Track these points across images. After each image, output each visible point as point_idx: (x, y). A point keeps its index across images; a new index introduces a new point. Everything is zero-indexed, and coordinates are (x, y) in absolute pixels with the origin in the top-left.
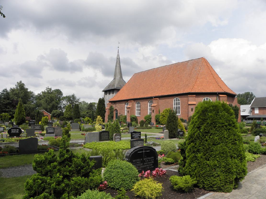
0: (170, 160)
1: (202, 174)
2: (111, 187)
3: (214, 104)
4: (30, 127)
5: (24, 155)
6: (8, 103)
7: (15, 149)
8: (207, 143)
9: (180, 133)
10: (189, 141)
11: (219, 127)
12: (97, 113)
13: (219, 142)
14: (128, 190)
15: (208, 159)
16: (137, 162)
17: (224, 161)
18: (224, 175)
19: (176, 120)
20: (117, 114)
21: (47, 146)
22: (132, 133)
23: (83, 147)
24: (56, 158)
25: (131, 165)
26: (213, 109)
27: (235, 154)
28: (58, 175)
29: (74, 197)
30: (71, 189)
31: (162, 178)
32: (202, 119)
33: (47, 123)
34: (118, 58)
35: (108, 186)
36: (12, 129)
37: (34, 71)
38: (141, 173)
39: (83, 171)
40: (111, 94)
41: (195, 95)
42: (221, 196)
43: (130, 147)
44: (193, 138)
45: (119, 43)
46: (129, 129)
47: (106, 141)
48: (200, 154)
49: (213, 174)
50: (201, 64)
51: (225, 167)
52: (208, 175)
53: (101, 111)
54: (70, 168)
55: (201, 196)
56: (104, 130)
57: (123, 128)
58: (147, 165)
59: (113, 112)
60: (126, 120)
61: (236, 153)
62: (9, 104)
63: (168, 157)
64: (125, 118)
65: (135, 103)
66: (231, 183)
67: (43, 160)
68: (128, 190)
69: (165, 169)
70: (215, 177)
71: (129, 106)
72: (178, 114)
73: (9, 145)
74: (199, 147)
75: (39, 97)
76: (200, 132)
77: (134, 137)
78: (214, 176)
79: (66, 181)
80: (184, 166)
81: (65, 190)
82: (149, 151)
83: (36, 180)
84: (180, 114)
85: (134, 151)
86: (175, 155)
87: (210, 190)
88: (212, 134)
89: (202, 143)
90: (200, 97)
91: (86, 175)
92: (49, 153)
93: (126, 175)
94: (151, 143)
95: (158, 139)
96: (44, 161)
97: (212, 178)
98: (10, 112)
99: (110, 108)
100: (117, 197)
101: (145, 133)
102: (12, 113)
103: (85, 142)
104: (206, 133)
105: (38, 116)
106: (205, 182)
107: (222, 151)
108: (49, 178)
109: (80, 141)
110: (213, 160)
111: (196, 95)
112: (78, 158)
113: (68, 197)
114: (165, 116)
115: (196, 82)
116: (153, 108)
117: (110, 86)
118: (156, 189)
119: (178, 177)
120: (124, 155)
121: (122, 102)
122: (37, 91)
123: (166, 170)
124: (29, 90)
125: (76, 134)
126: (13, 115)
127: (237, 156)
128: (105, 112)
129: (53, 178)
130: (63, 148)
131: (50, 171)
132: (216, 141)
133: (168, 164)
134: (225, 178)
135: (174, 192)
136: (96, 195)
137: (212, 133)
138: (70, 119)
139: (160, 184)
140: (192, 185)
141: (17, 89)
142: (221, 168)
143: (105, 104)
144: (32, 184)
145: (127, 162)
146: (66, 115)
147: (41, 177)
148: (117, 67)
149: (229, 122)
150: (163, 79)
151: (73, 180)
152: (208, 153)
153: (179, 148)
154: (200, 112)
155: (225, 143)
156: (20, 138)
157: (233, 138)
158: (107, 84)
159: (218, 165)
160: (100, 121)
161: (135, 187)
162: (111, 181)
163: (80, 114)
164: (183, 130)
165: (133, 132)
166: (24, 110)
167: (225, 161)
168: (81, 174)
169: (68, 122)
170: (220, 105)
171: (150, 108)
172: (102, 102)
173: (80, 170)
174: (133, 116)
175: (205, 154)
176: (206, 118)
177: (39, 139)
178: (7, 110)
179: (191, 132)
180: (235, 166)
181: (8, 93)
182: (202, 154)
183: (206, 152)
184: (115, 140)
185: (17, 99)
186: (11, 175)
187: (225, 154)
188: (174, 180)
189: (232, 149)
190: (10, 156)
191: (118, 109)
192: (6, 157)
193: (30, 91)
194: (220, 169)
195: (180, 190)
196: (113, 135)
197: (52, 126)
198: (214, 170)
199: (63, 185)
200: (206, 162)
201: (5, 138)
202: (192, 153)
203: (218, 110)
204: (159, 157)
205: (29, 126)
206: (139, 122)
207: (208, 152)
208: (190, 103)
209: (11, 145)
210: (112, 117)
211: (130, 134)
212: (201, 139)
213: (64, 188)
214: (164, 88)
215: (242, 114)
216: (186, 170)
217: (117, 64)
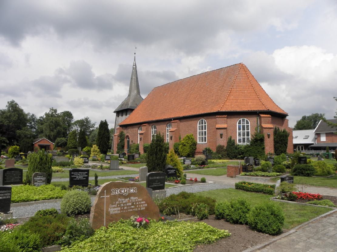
20: (128, 142)
34: (135, 68)
40: (124, 116)
45: (136, 48)
47: (13, 184)
59: (124, 139)
60: (139, 150)
65: (151, 127)
72: (204, 142)
75: (41, 122)
90: (234, 118)
99: (120, 134)
115: (229, 97)
146: (69, 145)
158: (120, 103)
185: (7, 124)
208: (218, 126)
215: (295, 141)
217: (133, 76)
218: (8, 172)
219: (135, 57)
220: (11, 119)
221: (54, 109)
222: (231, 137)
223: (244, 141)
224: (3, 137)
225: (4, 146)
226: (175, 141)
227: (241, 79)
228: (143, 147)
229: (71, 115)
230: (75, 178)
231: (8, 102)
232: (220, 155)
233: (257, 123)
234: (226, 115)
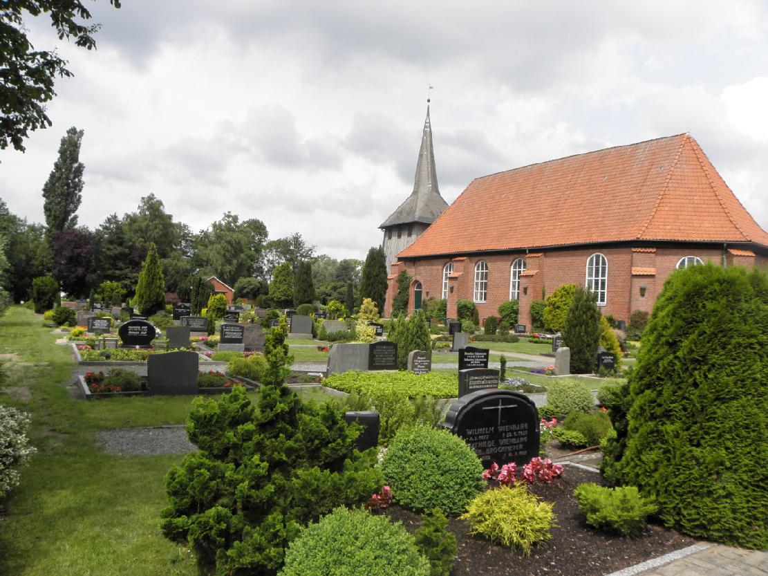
0: (574, 436)
1: (677, 486)
2: (401, 503)
3: (724, 273)
4: (177, 323)
5: (161, 397)
6: (121, 254)
7: (138, 379)
8: (697, 392)
9: (603, 358)
11: (740, 345)
12: (362, 288)
13: (735, 392)
14: (453, 515)
15: (695, 441)
16: (478, 436)
17: (749, 453)
18: (745, 493)
19: (595, 321)
20: (418, 294)
21: (223, 376)
22: (461, 352)
24: (253, 410)
25: (463, 443)
26: (722, 290)
28: (256, 458)
29: (298, 525)
30: (291, 502)
31: (548, 487)
33: (221, 312)
35: (394, 501)
36: (467, 352)
37: (202, 165)
38: (490, 469)
39: (328, 452)
42: (735, 559)
43: (457, 392)
44: (651, 376)
46: (453, 341)
47: (387, 369)
48: (672, 423)
49: (711, 489)
50: (679, 154)
51: (751, 471)
52: (695, 490)
54: (290, 443)
55: (671, 551)
56: (384, 338)
57: (436, 336)
58: (508, 445)
59: (408, 288)
60: (445, 313)
62: (121, 257)
63: (569, 428)
64: (443, 308)
65: (474, 264)
67: (215, 413)
68: (453, 515)
69: (560, 462)
70: (718, 497)
71: (453, 274)
73: (121, 367)
74: (671, 403)
75: (203, 240)
76: (677, 357)
77: (469, 362)
78: (715, 496)
79: (277, 476)
80: (618, 458)
81: (275, 504)
82: (515, 406)
83: (196, 470)
84: (605, 303)
85: (472, 402)
86: (591, 422)
88: (713, 365)
89: (680, 393)
91: (336, 465)
92: (231, 397)
93: (447, 472)
94: (519, 383)
96: (218, 416)
97: (707, 500)
98: (123, 279)
99: (399, 276)
100: (421, 534)
101: (500, 353)
103: (328, 370)
104: (695, 361)
105: (198, 294)
106: (682, 509)
107: (745, 420)
108: (232, 466)
110: (714, 446)
112: (313, 414)
113: (282, 522)
114: (558, 307)
116: (524, 282)
118: (535, 520)
119: (600, 489)
120: (439, 413)
123: (563, 466)
125: (301, 348)
126: (133, 289)
128: (386, 287)
129: (243, 466)
130: (271, 384)
131: (235, 446)
132: (726, 390)
133: (567, 446)
134: (750, 505)
135: (587, 531)
136: (362, 523)
137: (715, 362)
138: (286, 303)
139: (545, 505)
140: (642, 517)
142: (739, 471)
143: (387, 264)
144: (185, 480)
145: (451, 434)
147: (210, 463)
148: (424, 158)
151: (297, 477)
152: (699, 425)
153: (601, 402)
154: (680, 298)
155: (754, 396)
156: (152, 352)
158: (394, 209)
159: (728, 464)
161: (473, 509)
162: (404, 485)
163: (314, 291)
164: (612, 352)
165: (467, 348)
166: (162, 276)
167: (753, 453)
168: (321, 461)
169: (280, 314)
170: (744, 279)
172: (376, 258)
173: (318, 449)
174: (463, 302)
175: (688, 425)
177: (203, 357)
179: (647, 357)
181: (119, 228)
182: (678, 425)
184: (413, 370)
185: (142, 245)
186: (129, 449)
187: (754, 431)
188: (588, 497)
190: (125, 399)
192: (113, 401)
193: (180, 223)
194: (734, 476)
195: (605, 528)
197: (237, 321)
199: (271, 488)
200: (691, 451)
201: (112, 350)
202: (646, 421)
203: (739, 293)
204: (543, 427)
205: (173, 319)
206: (481, 322)
207: (699, 420)
208: (636, 270)
209: (128, 369)
210: (406, 304)
211: (458, 353)
213: (272, 497)
214: (560, 223)
216: (626, 470)
218: (378, 347)
219: (429, 107)
220: (148, 235)
221: (233, 214)
226: (533, 298)
229: (264, 228)
231: (143, 198)
234: (653, 247)
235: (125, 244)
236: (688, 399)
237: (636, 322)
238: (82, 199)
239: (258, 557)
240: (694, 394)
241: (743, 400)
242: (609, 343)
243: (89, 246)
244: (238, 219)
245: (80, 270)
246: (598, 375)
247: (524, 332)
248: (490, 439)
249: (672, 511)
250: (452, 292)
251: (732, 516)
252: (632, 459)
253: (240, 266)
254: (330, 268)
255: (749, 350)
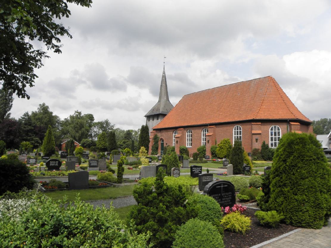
0: (246, 197)
1: (290, 209)
8: (294, 177)
10: (274, 175)
11: (307, 160)
18: (313, 210)
19: (242, 153)
20: (162, 144)
23: (137, 183)
26: (300, 142)
27: (324, 188)
32: (288, 152)
36: (51, 161)
41: (260, 122)
48: (287, 188)
53: (145, 141)
59: (158, 141)
61: (325, 188)
63: (242, 194)
64: (173, 150)
65: (186, 131)
66: (321, 219)
71: (177, 135)
72: (274, 147)
75: (66, 123)
76: (287, 165)
78: (303, 211)
85: (212, 186)
87: (298, 225)
95: (221, 175)
97: (301, 213)
98: (31, 140)
102: (35, 142)
104: (293, 166)
109: (134, 176)
111: (261, 122)
114: (222, 148)
117: (154, 111)
121: (169, 130)
122: (63, 115)
124: (53, 115)
127: (327, 191)
128: (149, 142)
134: (314, 214)
141: (40, 113)
142: (310, 202)
146: (98, 146)
148: (163, 87)
149: (318, 155)
150: (220, 102)
152: (296, 188)
154: (286, 145)
157: (322, 172)
158: (150, 108)
159: (307, 200)
160: (144, 152)
164: (249, 165)
165: (194, 166)
170: (307, 138)
171: (204, 137)
172: (145, 129)
174: (182, 147)
176: (292, 151)
178: (28, 139)
179: (276, 166)
180: (325, 201)
182: (289, 188)
183: (293, 187)
185: (40, 126)
187: (314, 189)
189: (321, 183)
190: (61, 191)
191: (164, 139)
196: (170, 169)
198: (302, 205)
201: (44, 172)
207: (296, 186)
208: (254, 132)
210: (157, 148)
212: (287, 173)
214: (221, 113)
221: (79, 111)
222: (264, 141)
223: (275, 145)
224: (37, 137)
225: (37, 145)
227: (271, 91)
228: (179, 149)
230: (195, 172)
231: (40, 105)
232: (256, 157)
233: (287, 130)
235: (32, 125)
236: (291, 179)
237: (254, 153)
238: (13, 106)
239: (166, 237)
240: (293, 177)
241: (310, 178)
242: (248, 162)
243: (16, 126)
244: (81, 113)
245: (12, 137)
246: (244, 175)
247: (209, 159)
248: (219, 198)
249: (289, 218)
250: (177, 143)
251: (309, 218)
252: (273, 201)
253: (83, 134)
254: (121, 134)
255: (310, 162)
